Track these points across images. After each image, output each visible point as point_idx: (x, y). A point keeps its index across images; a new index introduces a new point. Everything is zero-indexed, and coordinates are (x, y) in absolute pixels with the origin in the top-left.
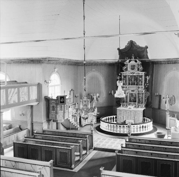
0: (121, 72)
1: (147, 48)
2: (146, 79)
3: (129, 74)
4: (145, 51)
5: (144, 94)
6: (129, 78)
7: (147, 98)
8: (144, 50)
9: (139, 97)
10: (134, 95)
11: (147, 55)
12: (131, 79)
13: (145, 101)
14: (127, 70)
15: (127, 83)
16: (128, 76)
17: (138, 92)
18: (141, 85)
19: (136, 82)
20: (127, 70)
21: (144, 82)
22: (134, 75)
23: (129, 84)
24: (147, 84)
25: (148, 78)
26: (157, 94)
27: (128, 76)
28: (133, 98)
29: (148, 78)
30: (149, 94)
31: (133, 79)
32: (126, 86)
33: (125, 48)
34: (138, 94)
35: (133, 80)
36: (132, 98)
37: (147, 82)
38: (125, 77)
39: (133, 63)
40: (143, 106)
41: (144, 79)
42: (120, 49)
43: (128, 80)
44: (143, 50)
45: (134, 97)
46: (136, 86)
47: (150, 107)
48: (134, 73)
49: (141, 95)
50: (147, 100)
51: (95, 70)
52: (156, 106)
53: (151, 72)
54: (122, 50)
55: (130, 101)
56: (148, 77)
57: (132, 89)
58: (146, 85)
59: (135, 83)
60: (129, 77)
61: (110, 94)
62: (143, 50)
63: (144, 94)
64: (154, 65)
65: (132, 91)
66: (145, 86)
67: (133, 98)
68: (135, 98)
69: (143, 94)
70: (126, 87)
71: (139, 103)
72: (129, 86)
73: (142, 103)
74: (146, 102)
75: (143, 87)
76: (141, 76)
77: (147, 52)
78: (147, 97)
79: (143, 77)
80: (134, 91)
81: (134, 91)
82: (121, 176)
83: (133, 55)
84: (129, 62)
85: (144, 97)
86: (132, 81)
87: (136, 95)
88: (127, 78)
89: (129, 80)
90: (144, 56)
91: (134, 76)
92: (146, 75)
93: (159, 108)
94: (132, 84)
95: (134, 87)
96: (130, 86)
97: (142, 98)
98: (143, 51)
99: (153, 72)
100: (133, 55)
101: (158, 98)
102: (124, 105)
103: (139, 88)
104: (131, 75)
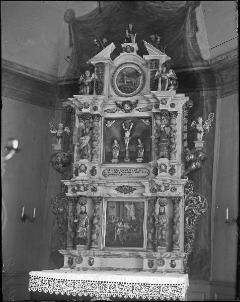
0: (92, 55)
5: (182, 203)
6: (107, 130)
9: (152, 217)
11: (194, 39)
12: (117, 133)
13: (186, 241)
14: (100, 92)
17: (153, 190)
19: (145, 147)
20: (100, 92)
21: (184, 148)
22: (135, 114)
28: (126, 226)
36: (119, 225)
37: (199, 144)
40: (179, 264)
41: (184, 132)
43: (101, 138)
45: (131, 222)
48: (133, 105)
49: (167, 209)
50: (194, 235)
55: (112, 241)
57: (124, 181)
61: (24, 219)
63: (182, 203)
65: (121, 189)
66: (187, 164)
67: (126, 226)
68: (137, 224)
69: (174, 201)
70: (93, 172)
71: (155, 250)
73: (171, 249)
79: (179, 124)
80: (130, 190)
81: (130, 190)
82: (2, 19)
83: (131, 27)
84: (114, 55)
85: (181, 219)
86: (122, 141)
88: (101, 131)
92: (192, 113)
94: (121, 159)
95: (129, 171)
97: (173, 223)
100: (131, 27)
102: (80, 260)
104: (121, 114)
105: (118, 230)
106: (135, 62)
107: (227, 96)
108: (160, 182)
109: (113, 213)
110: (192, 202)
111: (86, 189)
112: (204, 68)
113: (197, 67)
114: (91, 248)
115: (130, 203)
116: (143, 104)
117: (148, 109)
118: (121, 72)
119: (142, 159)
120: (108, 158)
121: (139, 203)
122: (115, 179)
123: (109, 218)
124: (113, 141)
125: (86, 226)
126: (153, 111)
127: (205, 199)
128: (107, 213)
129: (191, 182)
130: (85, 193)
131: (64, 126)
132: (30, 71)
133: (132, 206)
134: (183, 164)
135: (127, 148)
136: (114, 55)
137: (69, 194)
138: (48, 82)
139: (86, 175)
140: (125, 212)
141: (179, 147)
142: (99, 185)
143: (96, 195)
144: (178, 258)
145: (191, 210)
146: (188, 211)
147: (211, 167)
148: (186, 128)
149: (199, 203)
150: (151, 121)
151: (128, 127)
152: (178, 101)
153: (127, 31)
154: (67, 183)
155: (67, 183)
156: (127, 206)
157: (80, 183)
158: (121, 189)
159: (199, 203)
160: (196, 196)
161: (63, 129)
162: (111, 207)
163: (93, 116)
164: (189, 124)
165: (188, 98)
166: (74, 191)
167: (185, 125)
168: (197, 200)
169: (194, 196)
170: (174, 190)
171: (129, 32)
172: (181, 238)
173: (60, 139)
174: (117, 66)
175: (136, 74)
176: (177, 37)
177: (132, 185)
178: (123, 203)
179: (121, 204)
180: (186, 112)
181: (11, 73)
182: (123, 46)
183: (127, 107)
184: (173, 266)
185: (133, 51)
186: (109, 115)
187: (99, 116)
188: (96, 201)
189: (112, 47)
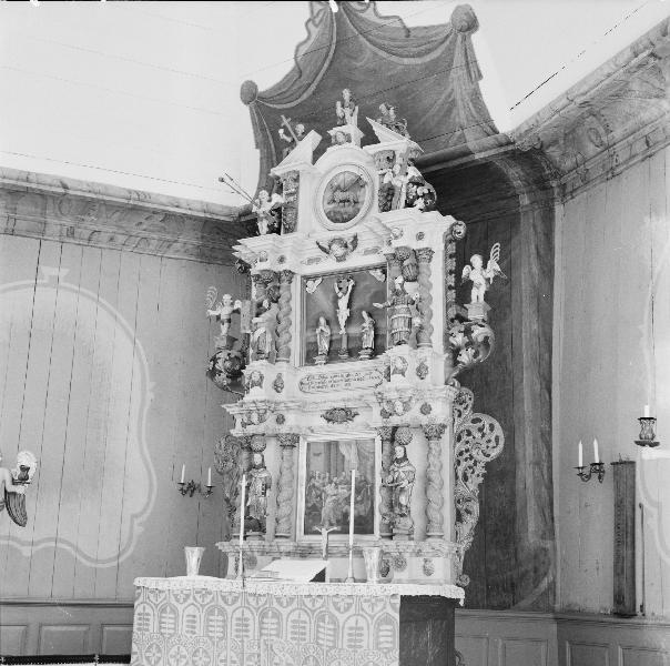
1: (471, 25)
2: (462, 290)
3: (310, 261)
4: (459, 59)
6: (308, 299)
7: (475, 481)
8: (450, 51)
9: (393, 489)
10: (351, 456)
11: (476, 96)
13: (459, 518)
15: (296, 347)
16: (297, 282)
18: (417, 338)
22: (356, 261)
23: (310, 356)
24: (467, 332)
25: (480, 273)
26: (588, 451)
27: (297, 282)
29: (480, 273)
30: (490, 441)
31: (343, 303)
32: (282, 367)
33: (299, 70)
34: (392, 437)
35: (344, 313)
36: (330, 489)
38: (275, 282)
39: (347, 157)
42: (262, 88)
43: (296, 316)
44: (434, 55)
46: (370, 363)
47: (535, 608)
50: (475, 507)
51: (64, 272)
52: (594, 593)
53: (535, 269)
54: (281, 92)
56: (476, 260)
57: (335, 398)
58: (459, 339)
59: (360, 338)
60: (312, 286)
62: (434, 55)
64: (559, 209)
65: (330, 416)
72: (312, 370)
74: (471, 521)
75: (435, 356)
76: (410, 262)
77: (473, 72)
78: (480, 470)
79: (437, 273)
80: (348, 415)
81: (348, 415)
83: (346, 94)
84: (318, 153)
87: (364, 456)
88: (296, 304)
89: (311, 323)
90: (449, 111)
91: (348, 274)
92: (460, 254)
93: (625, 608)
94: (332, 356)
96: (321, 369)
98: (441, 69)
99: (548, 272)
100: (346, 94)
101: (600, 498)
103: (388, 376)
104: (329, 265)
105: (328, 500)
106: (355, 162)
107: (573, 198)
108: (393, 395)
109: (319, 464)
110: (469, 434)
111: (261, 420)
112: (502, 150)
113: (478, 147)
114: (429, 536)
115: (348, 444)
116: (366, 242)
117: (376, 251)
118: (331, 184)
119: (369, 351)
120: (310, 356)
121: (365, 441)
122: (319, 397)
123: (310, 478)
124: (318, 321)
125: (264, 494)
126: (385, 252)
127: (497, 424)
128: (308, 466)
129: (464, 390)
130: (260, 429)
131: (233, 299)
132: (184, 205)
133: (354, 450)
134: (447, 355)
135: (343, 331)
136: (318, 153)
137: (237, 432)
138: (222, 218)
139: (263, 391)
140: (339, 462)
141: (438, 322)
142: (288, 409)
143: (284, 429)
144: (437, 552)
145: (467, 451)
146: (461, 454)
147: (547, 355)
148: (452, 280)
149: (483, 436)
150: (384, 272)
151: (344, 289)
152: (432, 229)
153: (339, 104)
154: (232, 409)
155: (232, 409)
156: (343, 450)
157: (252, 407)
158: (330, 416)
159: (483, 436)
160: (479, 420)
161: (232, 304)
162: (315, 455)
163: (278, 276)
164: (457, 272)
165: (450, 219)
166: (244, 425)
167: (451, 272)
168: (481, 430)
169: (474, 421)
170: (426, 410)
171: (343, 106)
172: (448, 513)
173: (543, 647)
174: (323, 173)
175: (358, 183)
176: (443, 97)
177: (350, 405)
178: (336, 444)
179: (332, 446)
180: (452, 248)
181: (154, 213)
182: (332, 132)
183: (338, 250)
184: (428, 572)
185: (349, 141)
186: (309, 270)
187: (291, 274)
188: (290, 442)
189: (313, 138)
